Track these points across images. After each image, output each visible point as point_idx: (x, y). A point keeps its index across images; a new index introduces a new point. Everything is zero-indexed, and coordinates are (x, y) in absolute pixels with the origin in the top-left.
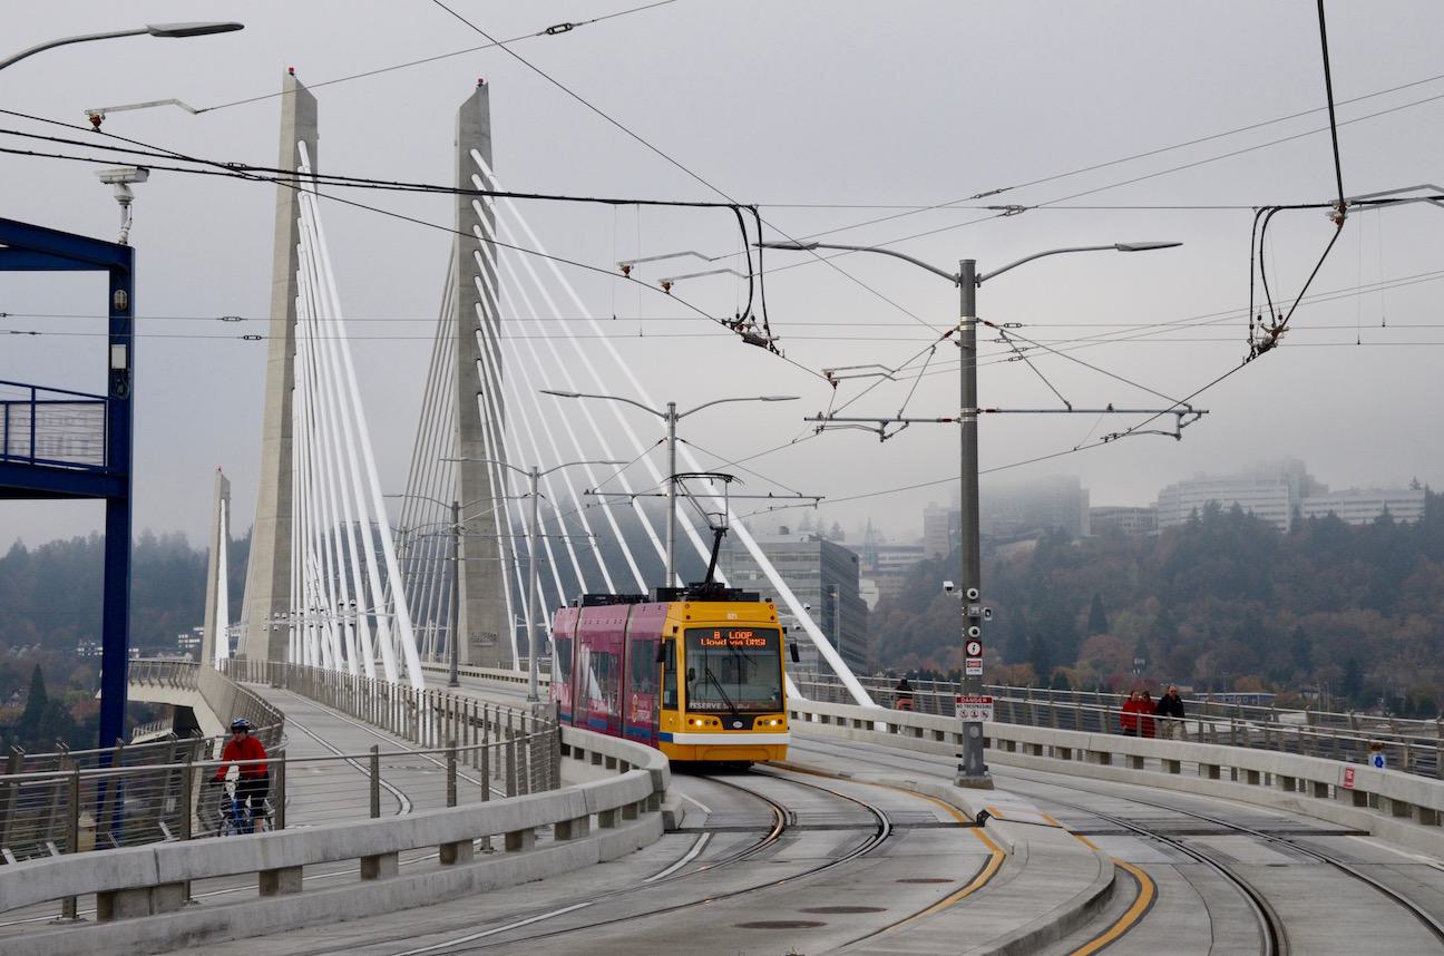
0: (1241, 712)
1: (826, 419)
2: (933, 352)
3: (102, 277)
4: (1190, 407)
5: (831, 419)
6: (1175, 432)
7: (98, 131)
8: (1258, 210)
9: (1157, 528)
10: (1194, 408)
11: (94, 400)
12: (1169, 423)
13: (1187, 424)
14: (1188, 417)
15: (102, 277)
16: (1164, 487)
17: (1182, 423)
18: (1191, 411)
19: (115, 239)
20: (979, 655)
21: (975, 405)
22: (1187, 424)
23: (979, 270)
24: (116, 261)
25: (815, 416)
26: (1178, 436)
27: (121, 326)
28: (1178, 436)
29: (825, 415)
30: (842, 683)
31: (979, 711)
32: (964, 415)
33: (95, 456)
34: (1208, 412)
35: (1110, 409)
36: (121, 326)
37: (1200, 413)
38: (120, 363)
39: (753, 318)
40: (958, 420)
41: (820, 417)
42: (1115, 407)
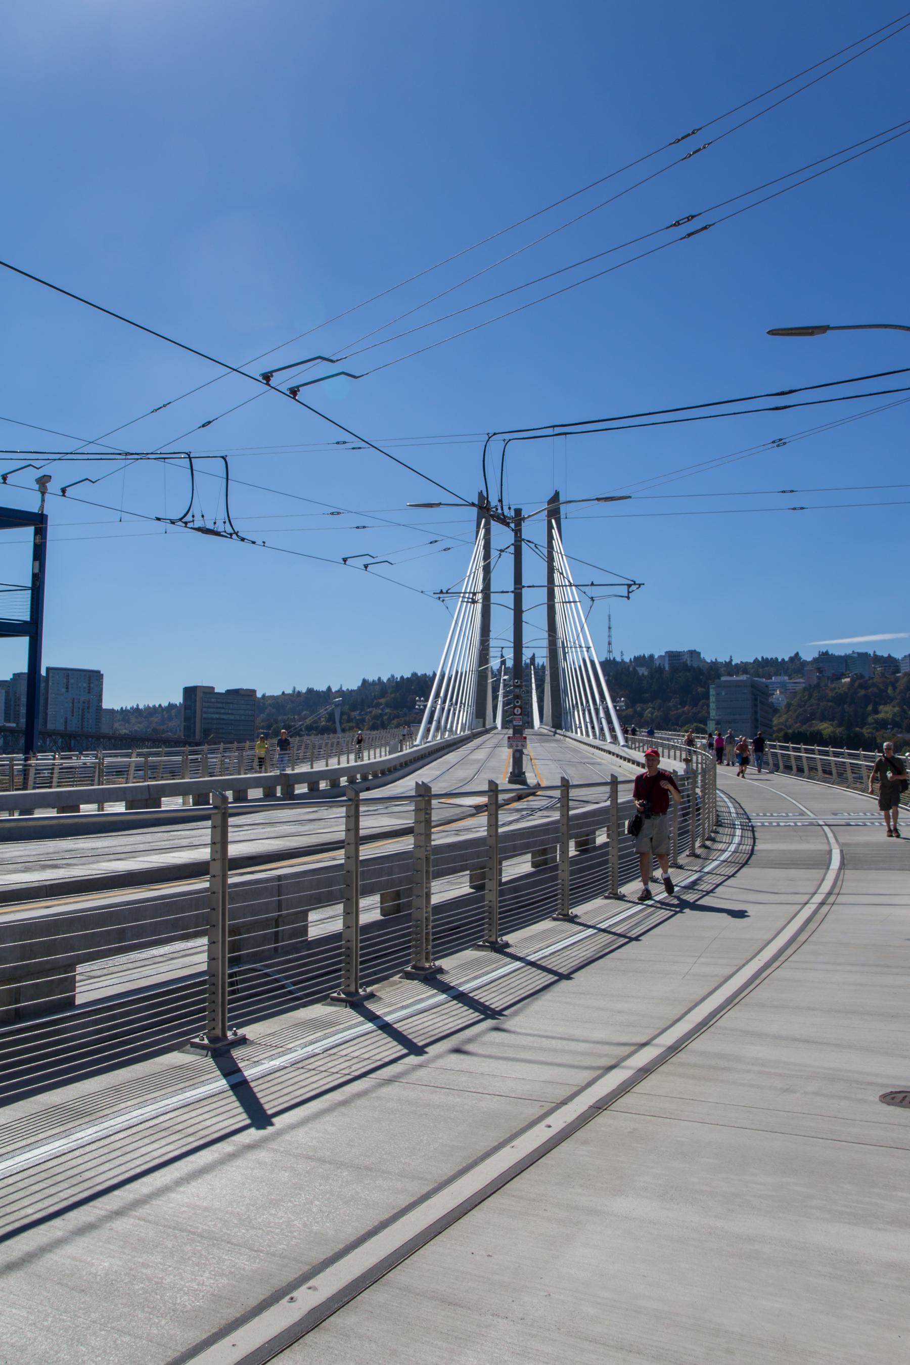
0: (846, 754)
1: (445, 593)
2: (500, 557)
3: (31, 529)
4: (635, 582)
5: (447, 593)
6: (627, 595)
7: (6, 483)
8: (506, 441)
9: (900, 673)
10: (637, 583)
11: (25, 588)
12: (623, 591)
13: (633, 591)
14: (634, 588)
15: (31, 529)
16: (903, 656)
17: (630, 590)
18: (635, 584)
19: (35, 510)
20: (520, 715)
21: (521, 583)
22: (633, 591)
23: (525, 514)
24: (38, 521)
25: (439, 592)
26: (628, 598)
27: (39, 553)
28: (628, 598)
29: (444, 591)
30: (624, 737)
31: (520, 744)
32: (521, 589)
33: (24, 615)
34: (644, 584)
35: (592, 584)
36: (39, 553)
37: (640, 585)
38: (37, 571)
39: (193, 516)
40: (512, 592)
41: (441, 592)
42: (595, 583)
